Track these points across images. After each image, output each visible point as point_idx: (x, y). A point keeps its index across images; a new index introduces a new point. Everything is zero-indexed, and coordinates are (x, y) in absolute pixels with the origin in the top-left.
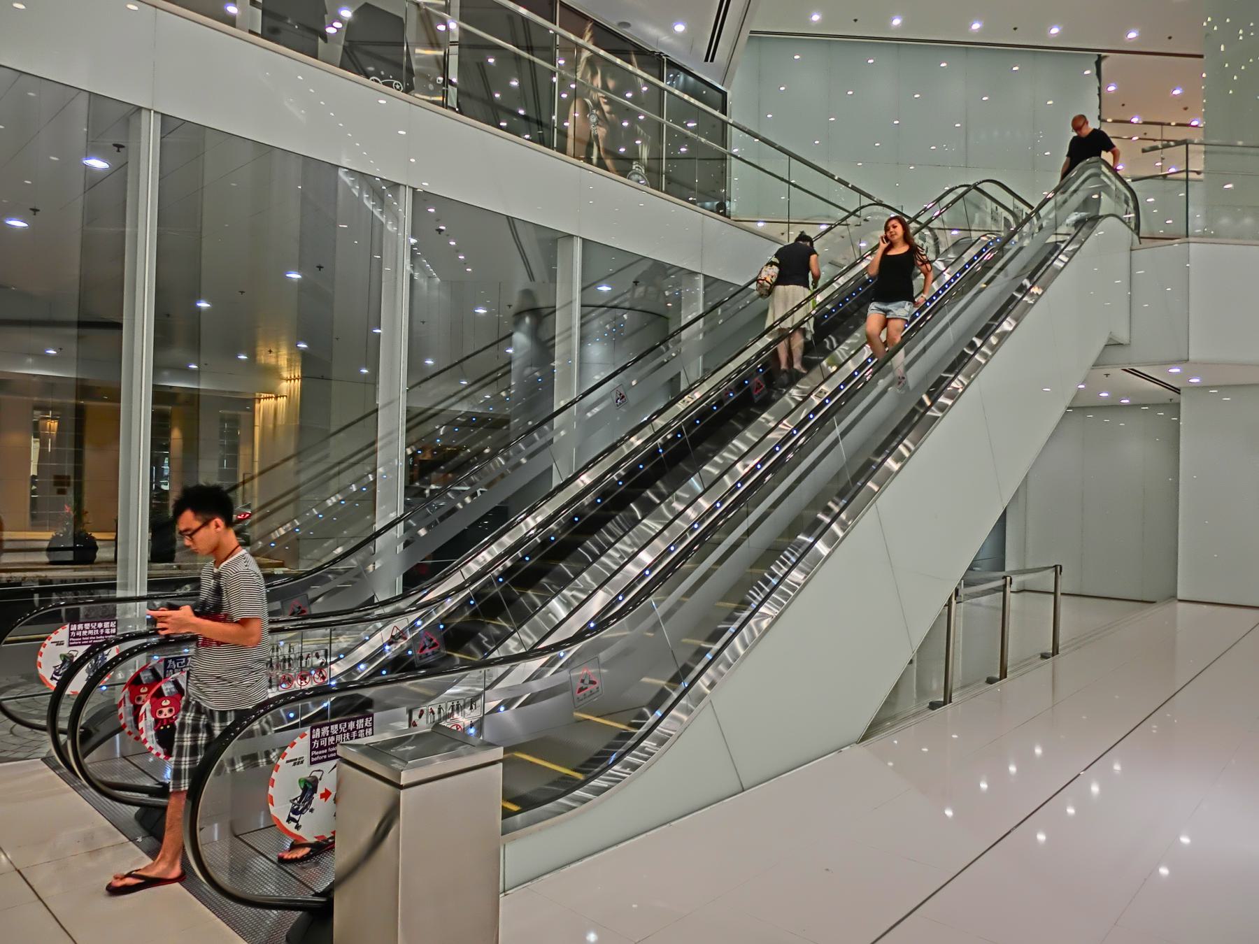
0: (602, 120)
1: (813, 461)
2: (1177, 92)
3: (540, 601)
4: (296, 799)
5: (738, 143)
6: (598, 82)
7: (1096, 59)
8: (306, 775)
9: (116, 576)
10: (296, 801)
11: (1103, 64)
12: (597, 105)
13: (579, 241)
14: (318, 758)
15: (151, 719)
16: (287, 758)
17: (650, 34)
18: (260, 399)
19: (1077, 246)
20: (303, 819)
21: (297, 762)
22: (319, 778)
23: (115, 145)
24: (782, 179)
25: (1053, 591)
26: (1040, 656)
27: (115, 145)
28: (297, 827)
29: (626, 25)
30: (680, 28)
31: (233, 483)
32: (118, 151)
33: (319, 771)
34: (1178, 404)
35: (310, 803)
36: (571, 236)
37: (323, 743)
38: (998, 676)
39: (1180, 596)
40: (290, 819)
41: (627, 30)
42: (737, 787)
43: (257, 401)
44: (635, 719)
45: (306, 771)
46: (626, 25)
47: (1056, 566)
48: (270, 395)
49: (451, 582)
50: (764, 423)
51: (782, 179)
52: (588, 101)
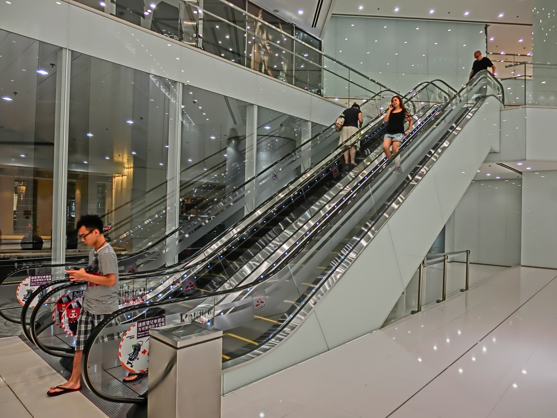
0: (266, 53)
1: (359, 204)
2: (521, 41)
3: (239, 266)
4: (131, 354)
5: (326, 64)
6: (264, 36)
7: (485, 26)
8: (135, 343)
9: (51, 255)
10: (131, 355)
11: (488, 28)
12: (264, 47)
13: (256, 107)
14: (141, 336)
15: (67, 318)
16: (127, 336)
17: (288, 15)
18: (115, 177)
19: (477, 109)
20: (134, 363)
21: (131, 337)
22: (141, 344)
23: (51, 64)
24: (346, 79)
25: (466, 262)
26: (460, 291)
27: (51, 64)
28: (132, 366)
29: (277, 11)
30: (301, 12)
31: (103, 214)
32: (52, 67)
33: (141, 341)
34: (521, 179)
35: (137, 356)
36: (253, 105)
37: (143, 329)
38: (441, 299)
39: (522, 264)
40: (128, 363)
41: (278, 13)
42: (326, 349)
43: (114, 177)
44: (281, 318)
45: (135, 341)
46: (277, 11)
47: (467, 251)
48: (120, 175)
49: (200, 258)
50: (338, 187)
51: (346, 79)
52: (260, 45)
